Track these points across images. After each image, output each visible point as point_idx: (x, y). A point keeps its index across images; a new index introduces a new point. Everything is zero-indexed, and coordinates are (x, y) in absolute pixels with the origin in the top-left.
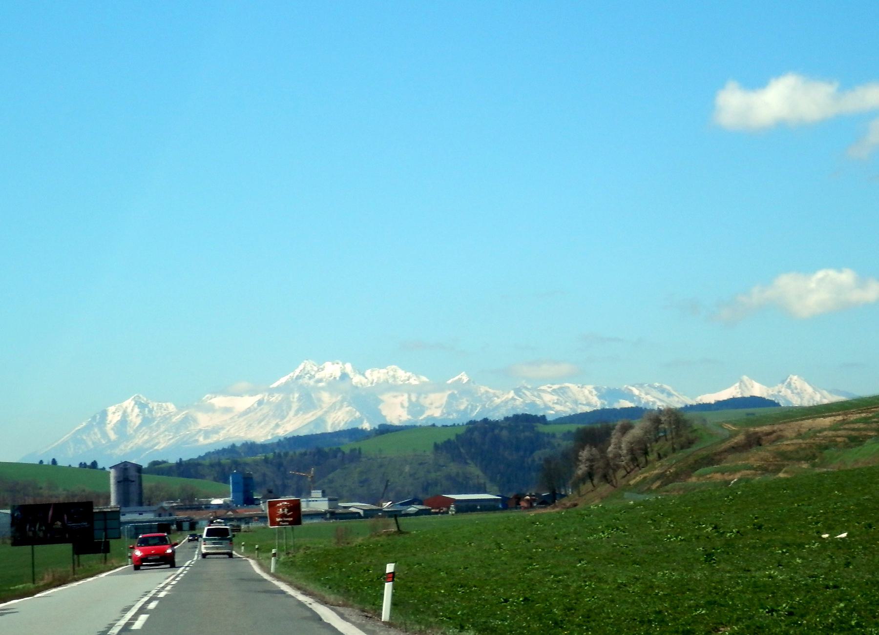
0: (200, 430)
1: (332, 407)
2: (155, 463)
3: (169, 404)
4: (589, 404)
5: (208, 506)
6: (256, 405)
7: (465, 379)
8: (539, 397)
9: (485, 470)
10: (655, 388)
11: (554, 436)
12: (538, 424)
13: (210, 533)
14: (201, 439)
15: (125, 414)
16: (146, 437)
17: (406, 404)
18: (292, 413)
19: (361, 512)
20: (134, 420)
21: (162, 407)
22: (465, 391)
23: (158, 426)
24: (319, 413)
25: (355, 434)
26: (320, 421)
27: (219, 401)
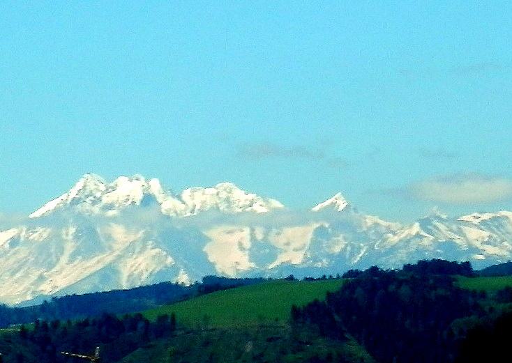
1: (130, 250)
6: (7, 246)
7: (342, 204)
8: (460, 232)
11: (483, 295)
12: (459, 277)
17: (247, 244)
18: (64, 259)
22: (341, 222)
24: (108, 258)
25: (164, 291)
26: (110, 271)
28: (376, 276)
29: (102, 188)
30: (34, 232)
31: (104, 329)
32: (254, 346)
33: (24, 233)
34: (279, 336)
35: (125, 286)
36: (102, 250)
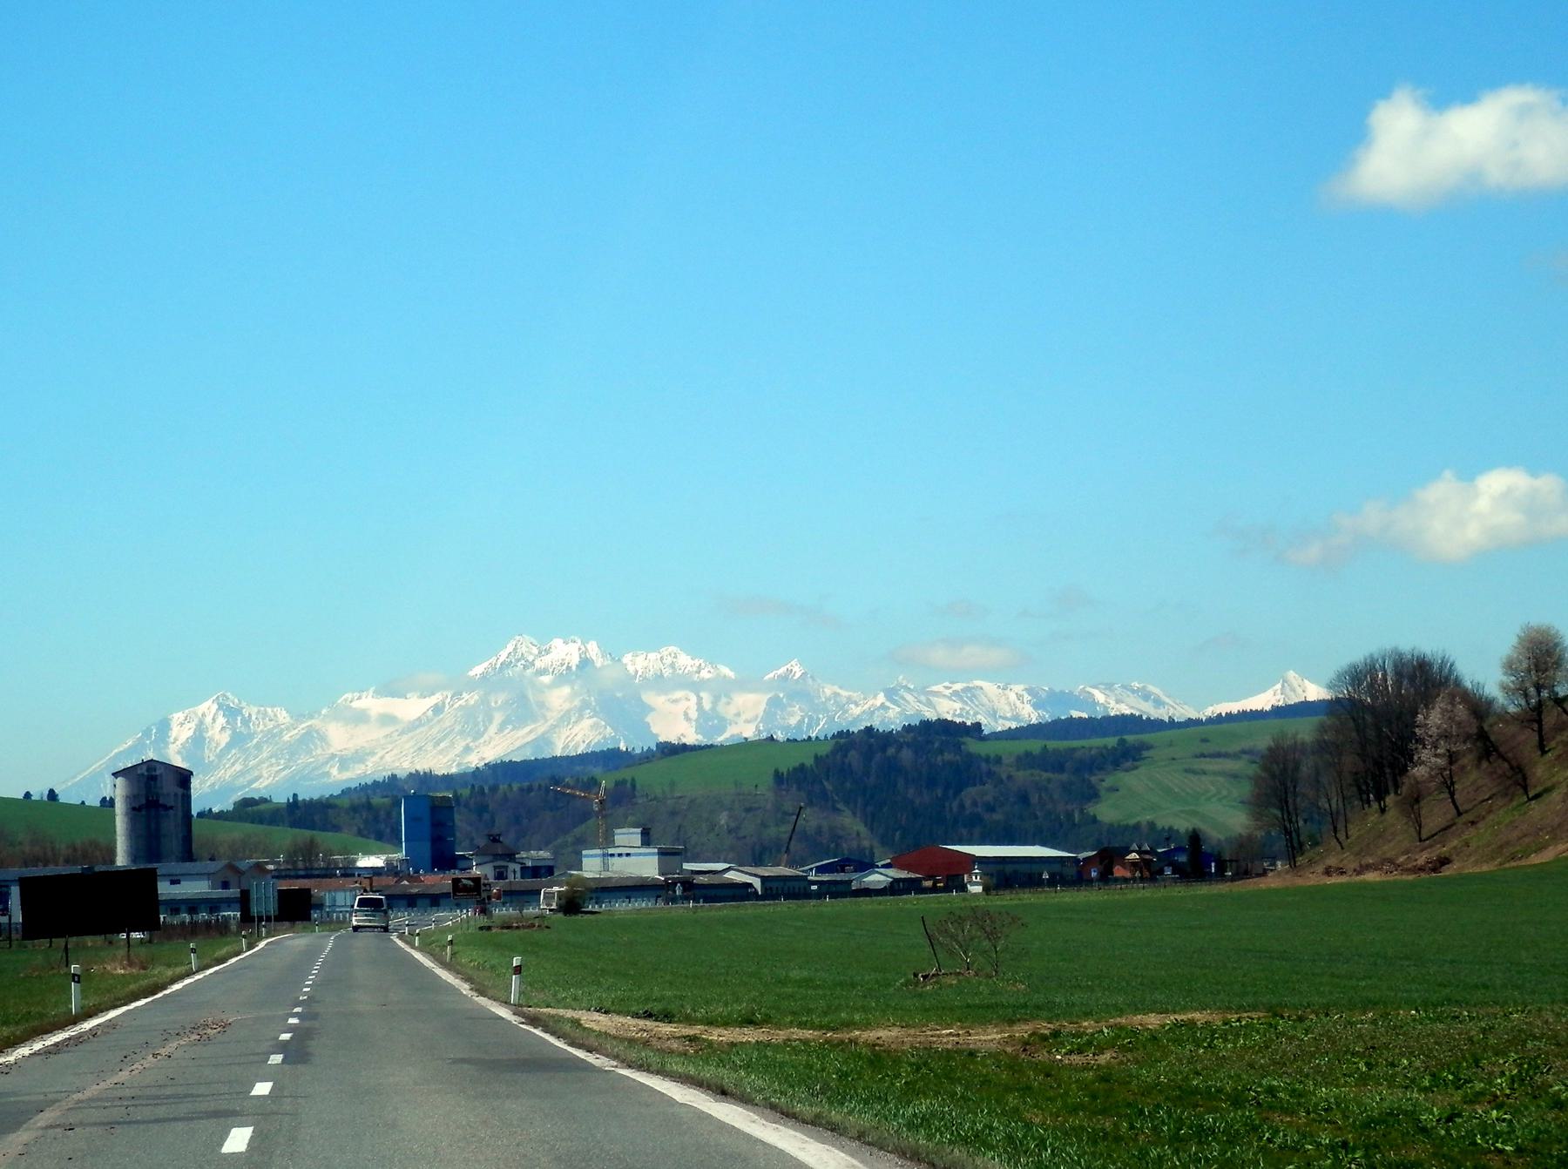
0: (333, 756)
1: (565, 718)
4: (1016, 718)
5: (349, 872)
6: (430, 713)
7: (798, 671)
8: (930, 704)
9: (871, 821)
10: (1133, 691)
11: (998, 760)
12: (968, 740)
14: (334, 771)
15: (200, 729)
16: (238, 767)
17: (694, 714)
18: (493, 729)
19: (757, 883)
20: (217, 737)
22: (798, 691)
23: (258, 747)
25: (611, 758)
26: (544, 740)
27: (371, 704)
29: (535, 651)
32: (730, 817)
36: (535, 721)
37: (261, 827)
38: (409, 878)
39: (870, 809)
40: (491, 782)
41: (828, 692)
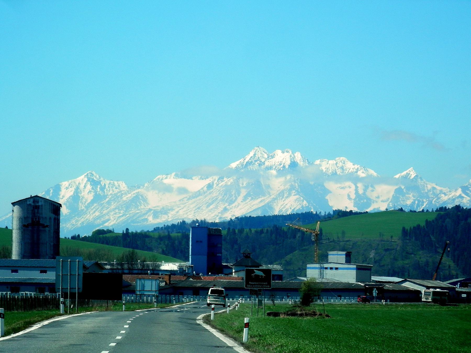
0: (150, 210)
1: (281, 194)
2: (100, 232)
3: (120, 183)
5: (156, 272)
6: (205, 189)
9: (456, 260)
13: (213, 292)
16: (97, 214)
17: (353, 196)
18: (240, 199)
20: (86, 196)
21: (114, 185)
22: (411, 185)
23: (109, 203)
24: (267, 200)
25: (308, 217)
26: (269, 206)
27: (170, 180)
28: (460, 211)
29: (266, 156)
30: (222, 181)
31: (274, 235)
32: (376, 254)
33: (216, 181)
34: (392, 248)
35: (276, 213)
36: (264, 195)
37: (107, 246)
38: (193, 277)
39: (456, 253)
40: (239, 227)
41: (429, 187)
